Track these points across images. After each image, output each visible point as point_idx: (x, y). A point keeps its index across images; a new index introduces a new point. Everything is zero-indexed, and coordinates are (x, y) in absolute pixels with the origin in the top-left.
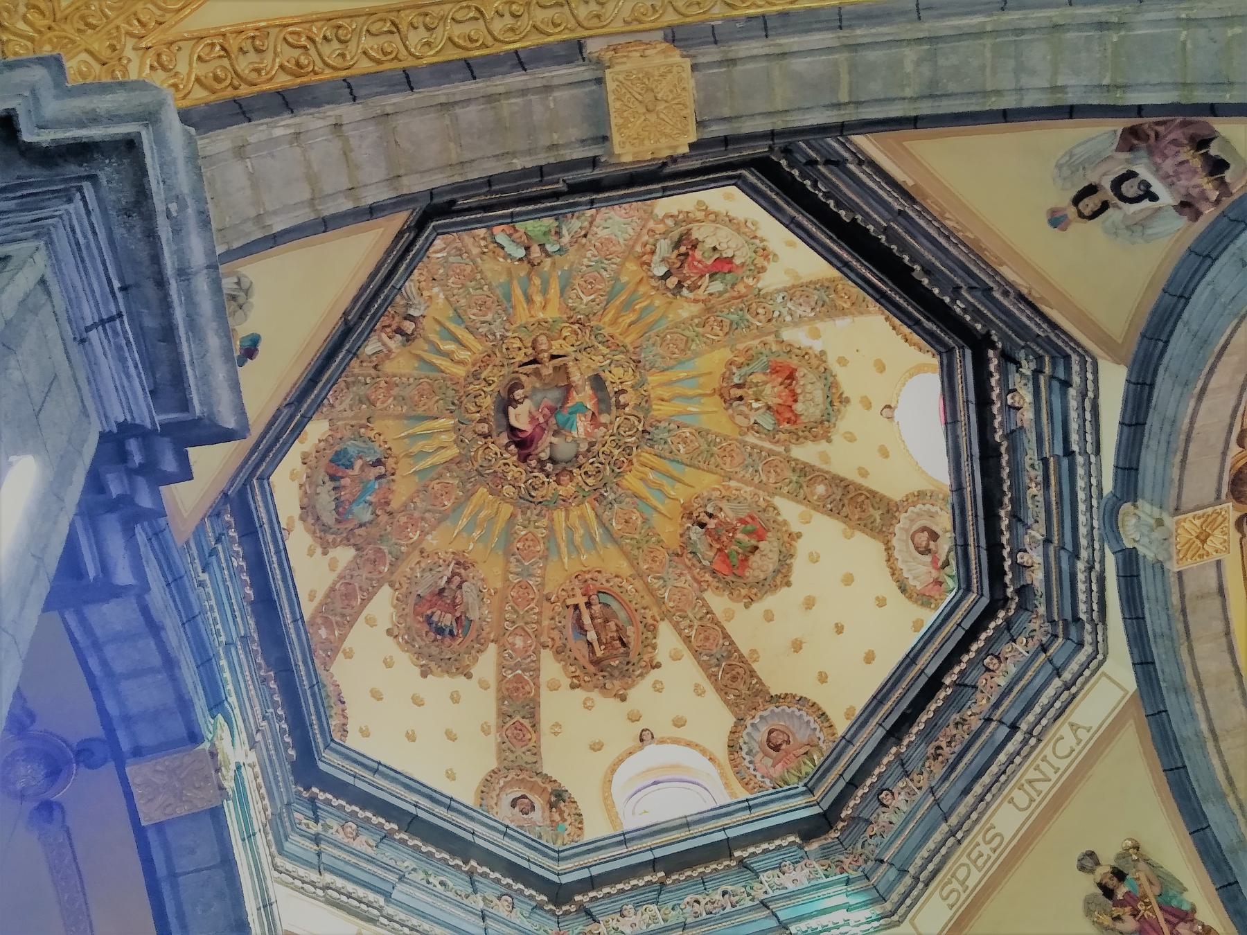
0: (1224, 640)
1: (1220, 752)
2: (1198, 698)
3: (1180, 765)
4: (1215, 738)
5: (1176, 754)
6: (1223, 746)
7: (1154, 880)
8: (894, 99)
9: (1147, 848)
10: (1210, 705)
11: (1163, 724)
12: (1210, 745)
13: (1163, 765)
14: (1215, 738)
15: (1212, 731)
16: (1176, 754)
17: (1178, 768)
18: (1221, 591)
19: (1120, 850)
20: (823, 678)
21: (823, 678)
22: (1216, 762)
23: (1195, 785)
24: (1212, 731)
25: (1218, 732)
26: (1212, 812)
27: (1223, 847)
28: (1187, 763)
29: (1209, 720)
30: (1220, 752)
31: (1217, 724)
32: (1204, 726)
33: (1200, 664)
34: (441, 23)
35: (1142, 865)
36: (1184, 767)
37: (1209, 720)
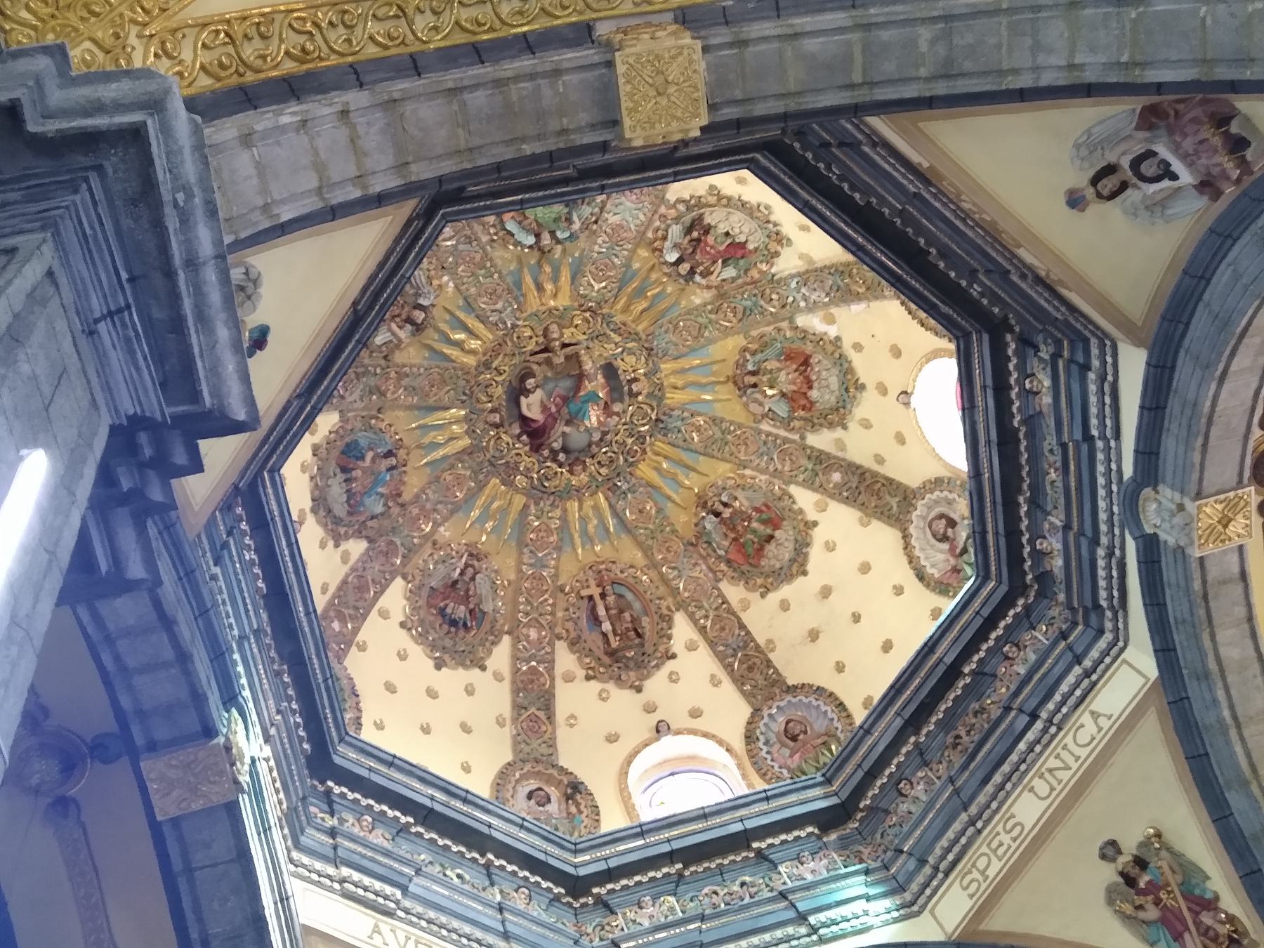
0: (1246, 626)
1: (1242, 739)
2: (1220, 684)
3: (1202, 752)
6: (1246, 733)
7: (1176, 868)
9: (1169, 837)
10: (1233, 692)
13: (1185, 753)
15: (1235, 717)
19: (1142, 839)
24: (1235, 717)
26: (1234, 799)
29: (1232, 707)
30: (1242, 739)
32: (1226, 713)
33: (1223, 651)
35: (1164, 853)
36: (1207, 754)
37: (1232, 707)
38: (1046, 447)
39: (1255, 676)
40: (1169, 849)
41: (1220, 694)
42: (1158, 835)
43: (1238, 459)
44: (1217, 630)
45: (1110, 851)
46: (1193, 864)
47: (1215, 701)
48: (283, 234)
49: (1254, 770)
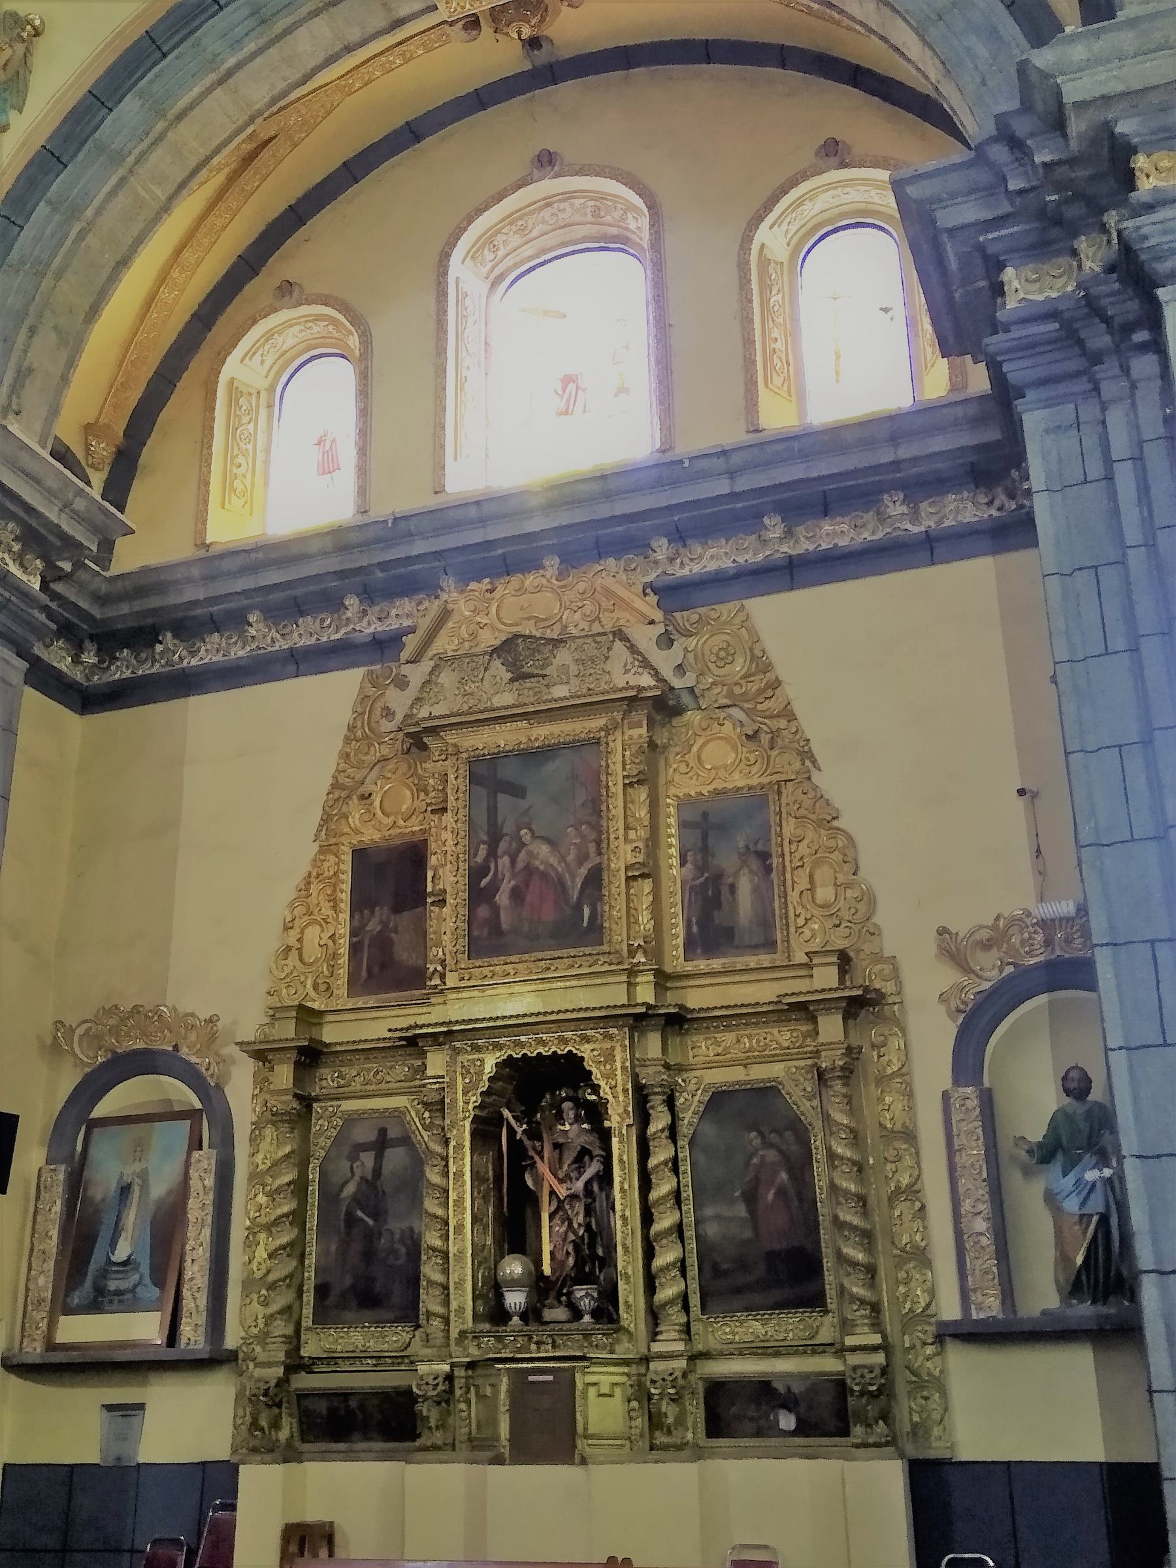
0: (339, 46)
1: (209, 90)
2: (262, 42)
3: (165, 49)
4: (221, 82)
5: (177, 38)
6: (218, 92)
7: (11, 70)
8: (970, 534)
9: (40, 44)
10: (258, 61)
11: (204, 11)
12: (212, 77)
13: (154, 27)
14: (221, 82)
15: (230, 73)
16: (177, 38)
17: (159, 48)
18: (399, 23)
19: (22, 14)
20: (622, 390)
21: (622, 390)
22: (196, 91)
23: (150, 75)
24: (230, 73)
25: (231, 81)
26: (130, 108)
27: (97, 135)
28: (169, 57)
29: (239, 66)
30: (209, 90)
31: (240, 75)
32: (232, 61)
33: (301, 32)
34: (969, 155)
35: (20, 48)
36: (165, 56)
37: (239, 66)
38: (762, 957)
39: (285, 79)
40: (27, 53)
41: (251, 47)
42: (37, 34)
43: (1160, 968)
44: (324, 15)
45: (545, 159)
46: (26, 86)
47: (237, 43)
48: (83, 1371)
49: (181, 116)
